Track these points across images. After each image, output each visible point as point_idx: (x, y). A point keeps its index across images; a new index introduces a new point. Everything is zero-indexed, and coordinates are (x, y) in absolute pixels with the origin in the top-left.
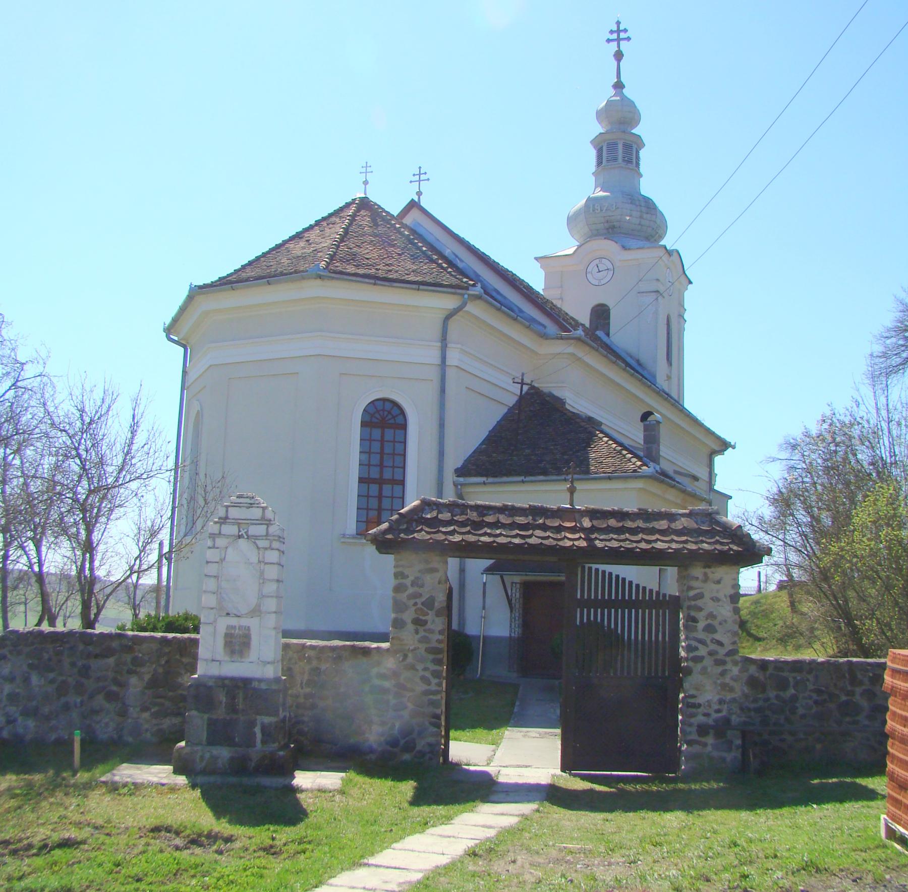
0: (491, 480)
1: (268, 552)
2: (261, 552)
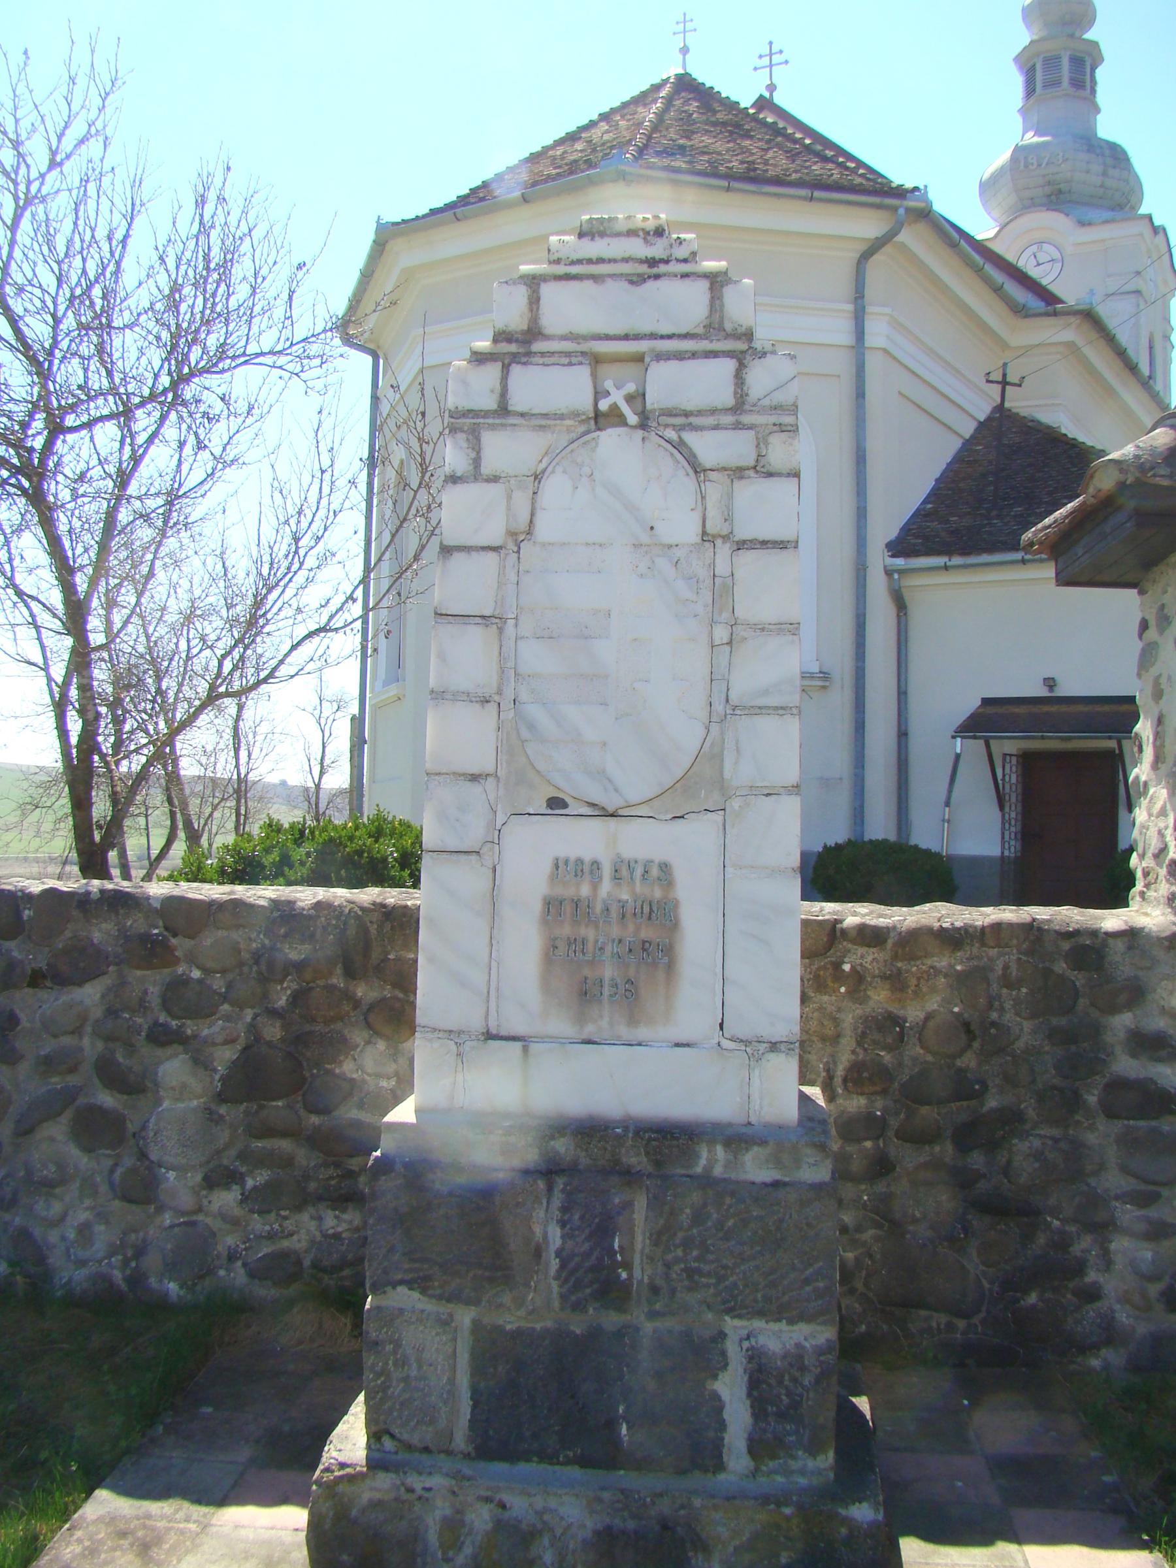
0: (957, 560)
1: (748, 492)
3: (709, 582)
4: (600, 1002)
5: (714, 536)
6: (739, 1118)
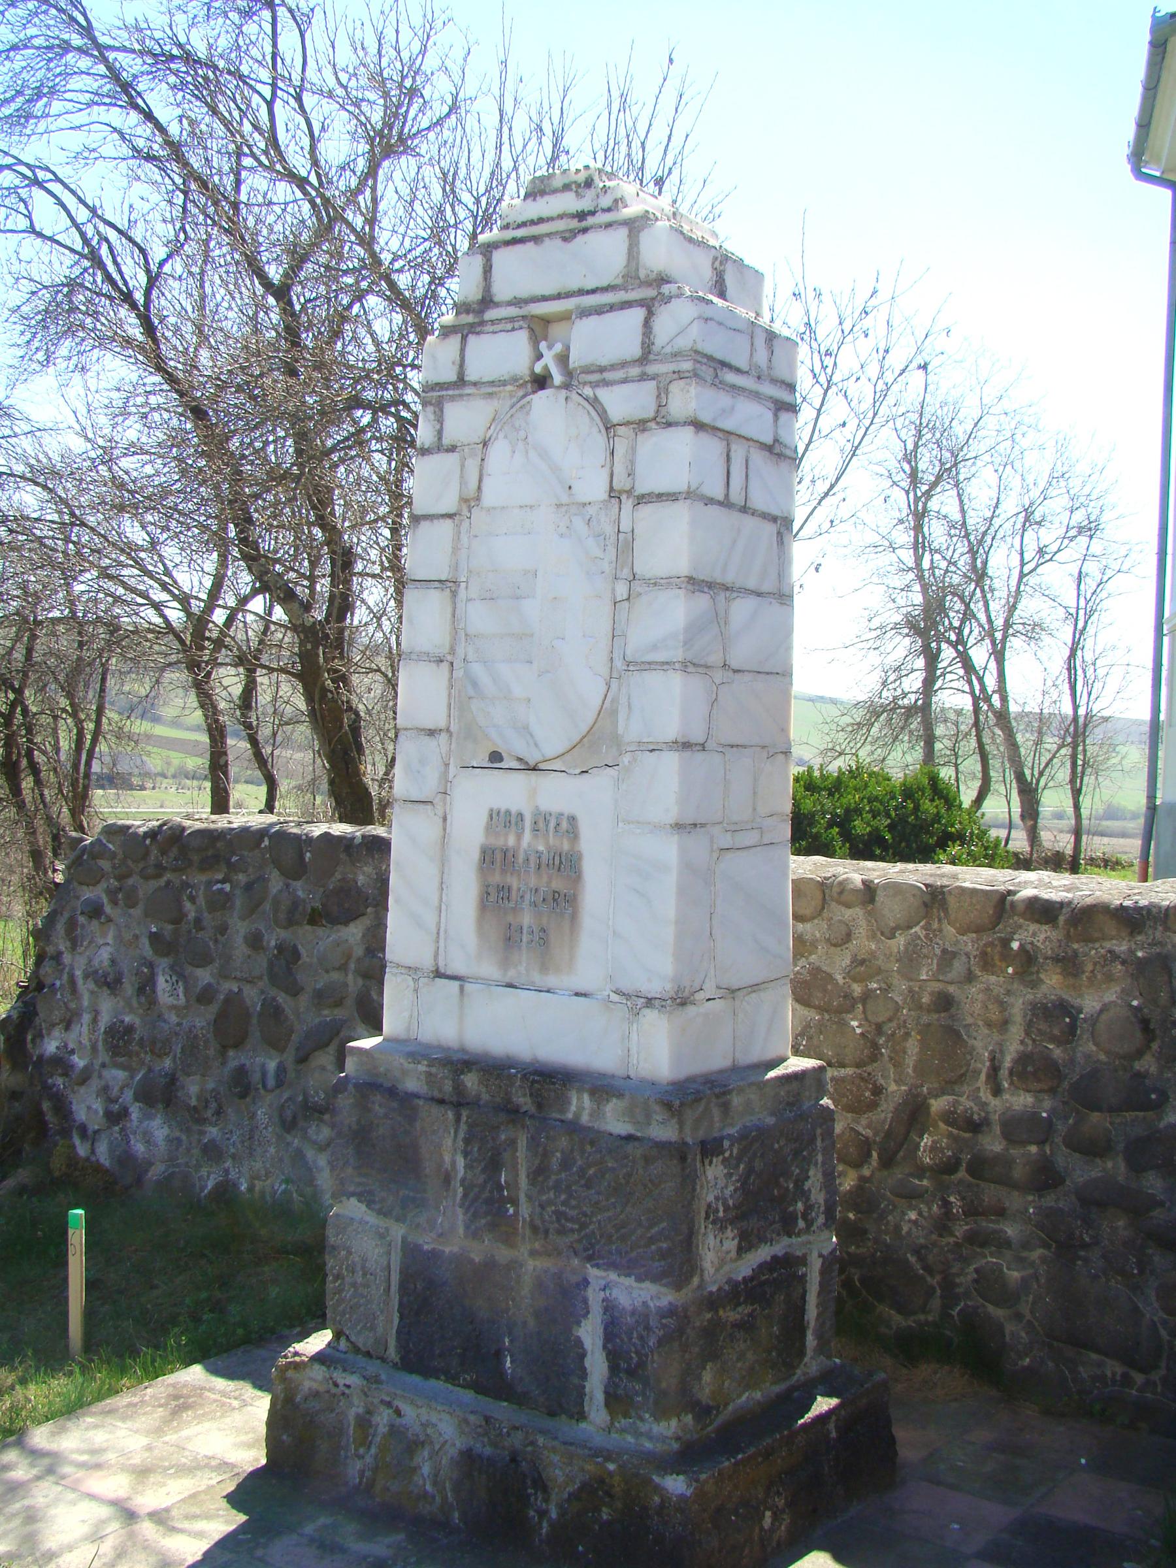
1: (654, 443)
2: (621, 448)
3: (613, 538)
4: (520, 948)
5: (620, 492)
6: (621, 1072)
